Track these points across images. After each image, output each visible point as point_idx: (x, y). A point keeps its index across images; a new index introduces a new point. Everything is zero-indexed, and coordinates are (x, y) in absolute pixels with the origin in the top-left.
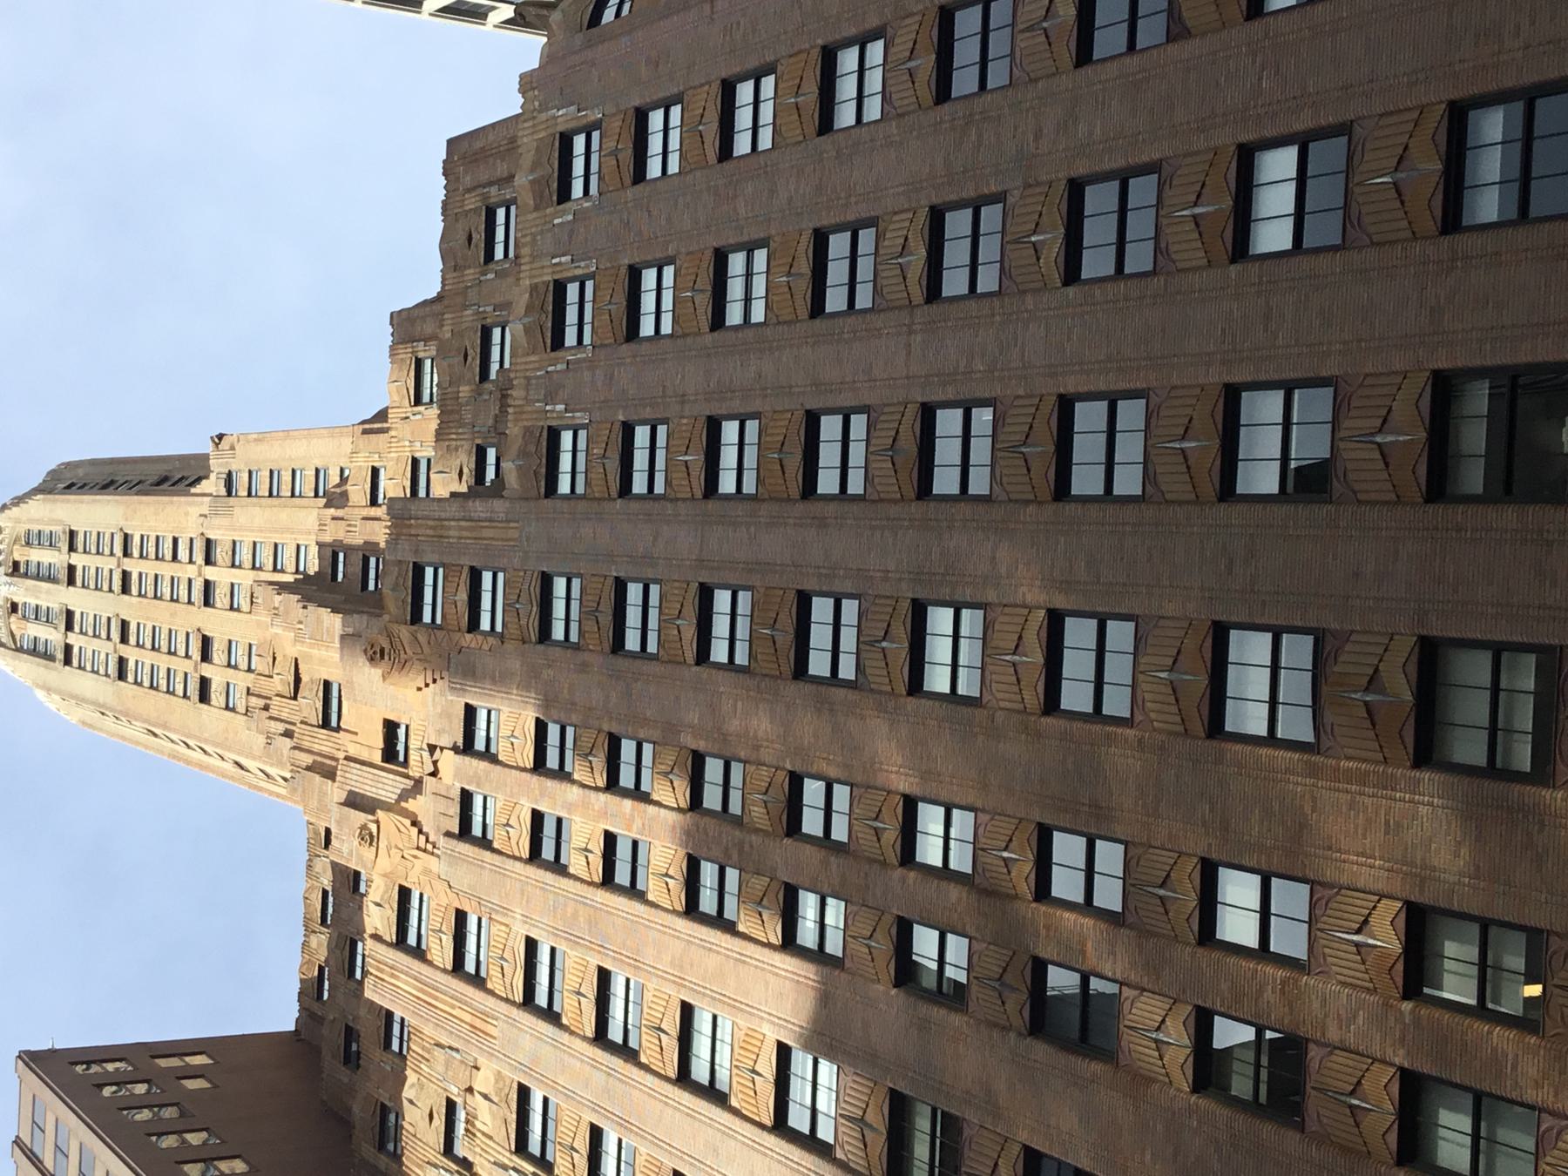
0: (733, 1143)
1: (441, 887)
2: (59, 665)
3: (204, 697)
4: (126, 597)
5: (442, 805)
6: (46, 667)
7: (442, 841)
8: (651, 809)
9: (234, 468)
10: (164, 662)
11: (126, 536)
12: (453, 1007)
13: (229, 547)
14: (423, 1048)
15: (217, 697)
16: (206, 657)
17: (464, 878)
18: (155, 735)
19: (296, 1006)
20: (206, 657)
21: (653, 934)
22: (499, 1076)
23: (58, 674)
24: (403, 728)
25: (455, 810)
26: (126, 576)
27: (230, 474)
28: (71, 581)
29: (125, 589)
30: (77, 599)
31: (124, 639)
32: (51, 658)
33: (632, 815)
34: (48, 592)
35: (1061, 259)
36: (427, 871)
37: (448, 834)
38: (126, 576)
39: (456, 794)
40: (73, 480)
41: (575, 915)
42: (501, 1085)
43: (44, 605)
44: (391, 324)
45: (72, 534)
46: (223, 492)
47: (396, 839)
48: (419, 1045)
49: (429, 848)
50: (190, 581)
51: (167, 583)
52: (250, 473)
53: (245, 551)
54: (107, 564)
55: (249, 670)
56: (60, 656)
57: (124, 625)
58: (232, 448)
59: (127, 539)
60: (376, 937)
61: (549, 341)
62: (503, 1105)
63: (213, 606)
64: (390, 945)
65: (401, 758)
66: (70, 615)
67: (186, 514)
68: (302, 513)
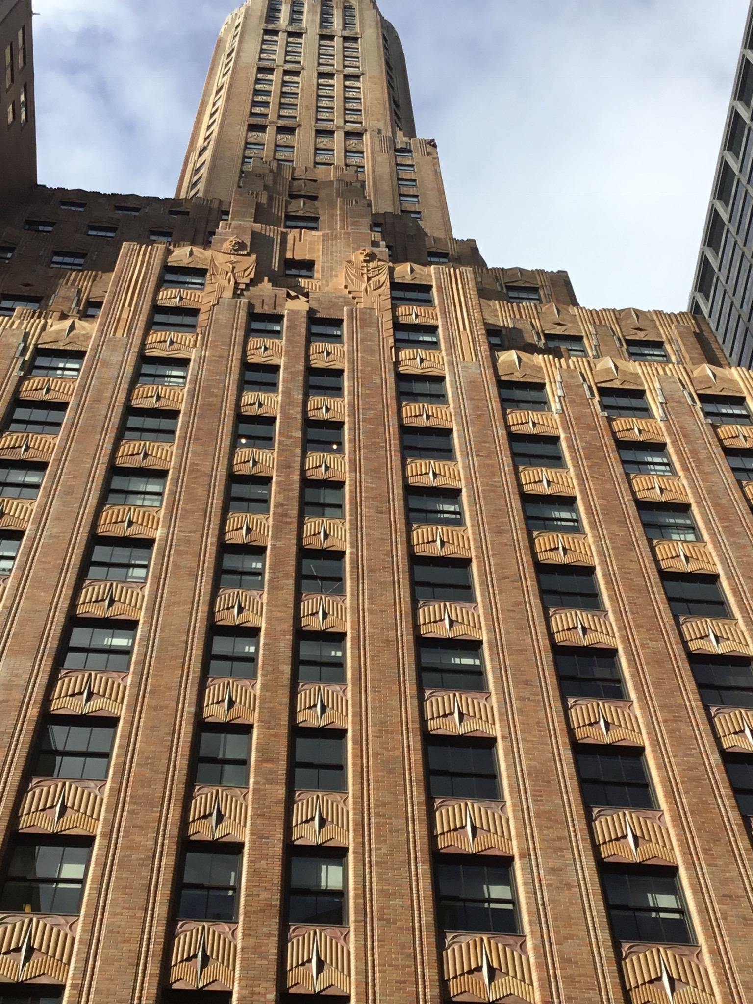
0: (77, 505)
1: (213, 300)
2: (263, 25)
3: (252, 128)
4: (315, 75)
5: (269, 301)
6: (261, 17)
7: (244, 300)
8: (298, 451)
9: (414, 155)
10: (273, 100)
11: (359, 77)
12: (130, 305)
13: (329, 146)
14: (74, 281)
15: (253, 136)
16: (281, 130)
17: (222, 316)
18: (218, 92)
19: (55, 186)
20: (281, 130)
21: (211, 449)
22: (87, 337)
23: (257, 25)
24: (308, 274)
25: (267, 310)
26: (330, 75)
27: (410, 151)
28: (322, 37)
29: (321, 75)
30: (309, 44)
31: (286, 73)
32: (322, 26)
33: (291, 437)
34: (313, 21)
35: (737, 750)
36: (222, 289)
37: (251, 306)
38: (330, 75)
39: (278, 311)
40: (389, 38)
41: (212, 395)
42: (81, 338)
43: (305, 17)
44: (559, 272)
45: (355, 39)
46: (398, 146)
47: (239, 268)
48: (76, 276)
49: (237, 293)
50: (333, 120)
51: (329, 104)
52: (412, 166)
53: (357, 160)
54: (279, 58)
55: (316, 163)
56: (270, 27)
57: (296, 73)
58: (428, 154)
59: (356, 77)
60: (168, 252)
61: (603, 385)
62: (68, 340)
63: (316, 137)
64: (165, 261)
65: (288, 272)
66: (299, 35)
67: (378, 120)
68: (389, 202)
